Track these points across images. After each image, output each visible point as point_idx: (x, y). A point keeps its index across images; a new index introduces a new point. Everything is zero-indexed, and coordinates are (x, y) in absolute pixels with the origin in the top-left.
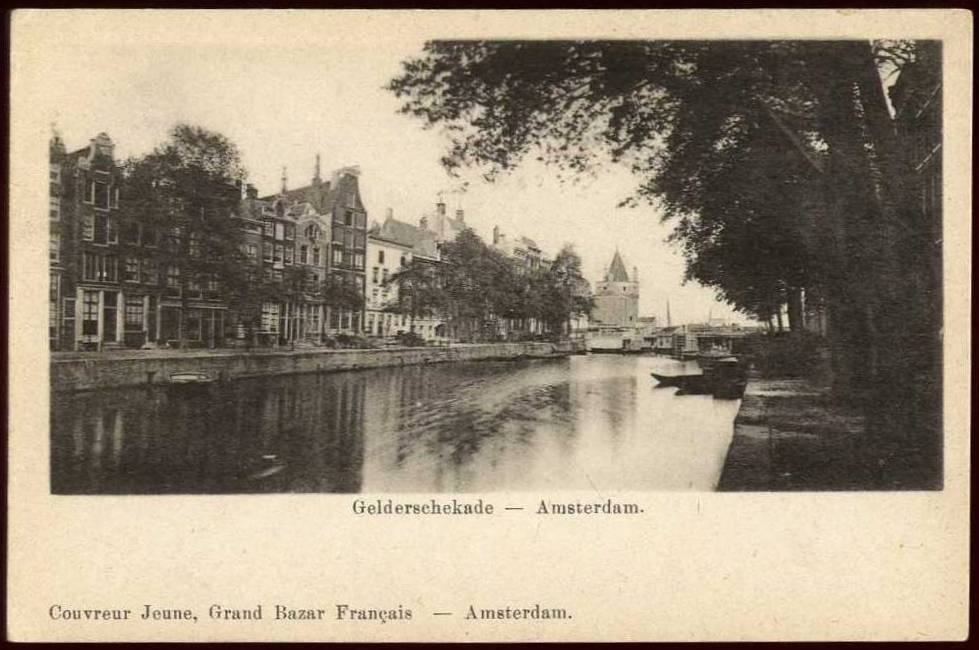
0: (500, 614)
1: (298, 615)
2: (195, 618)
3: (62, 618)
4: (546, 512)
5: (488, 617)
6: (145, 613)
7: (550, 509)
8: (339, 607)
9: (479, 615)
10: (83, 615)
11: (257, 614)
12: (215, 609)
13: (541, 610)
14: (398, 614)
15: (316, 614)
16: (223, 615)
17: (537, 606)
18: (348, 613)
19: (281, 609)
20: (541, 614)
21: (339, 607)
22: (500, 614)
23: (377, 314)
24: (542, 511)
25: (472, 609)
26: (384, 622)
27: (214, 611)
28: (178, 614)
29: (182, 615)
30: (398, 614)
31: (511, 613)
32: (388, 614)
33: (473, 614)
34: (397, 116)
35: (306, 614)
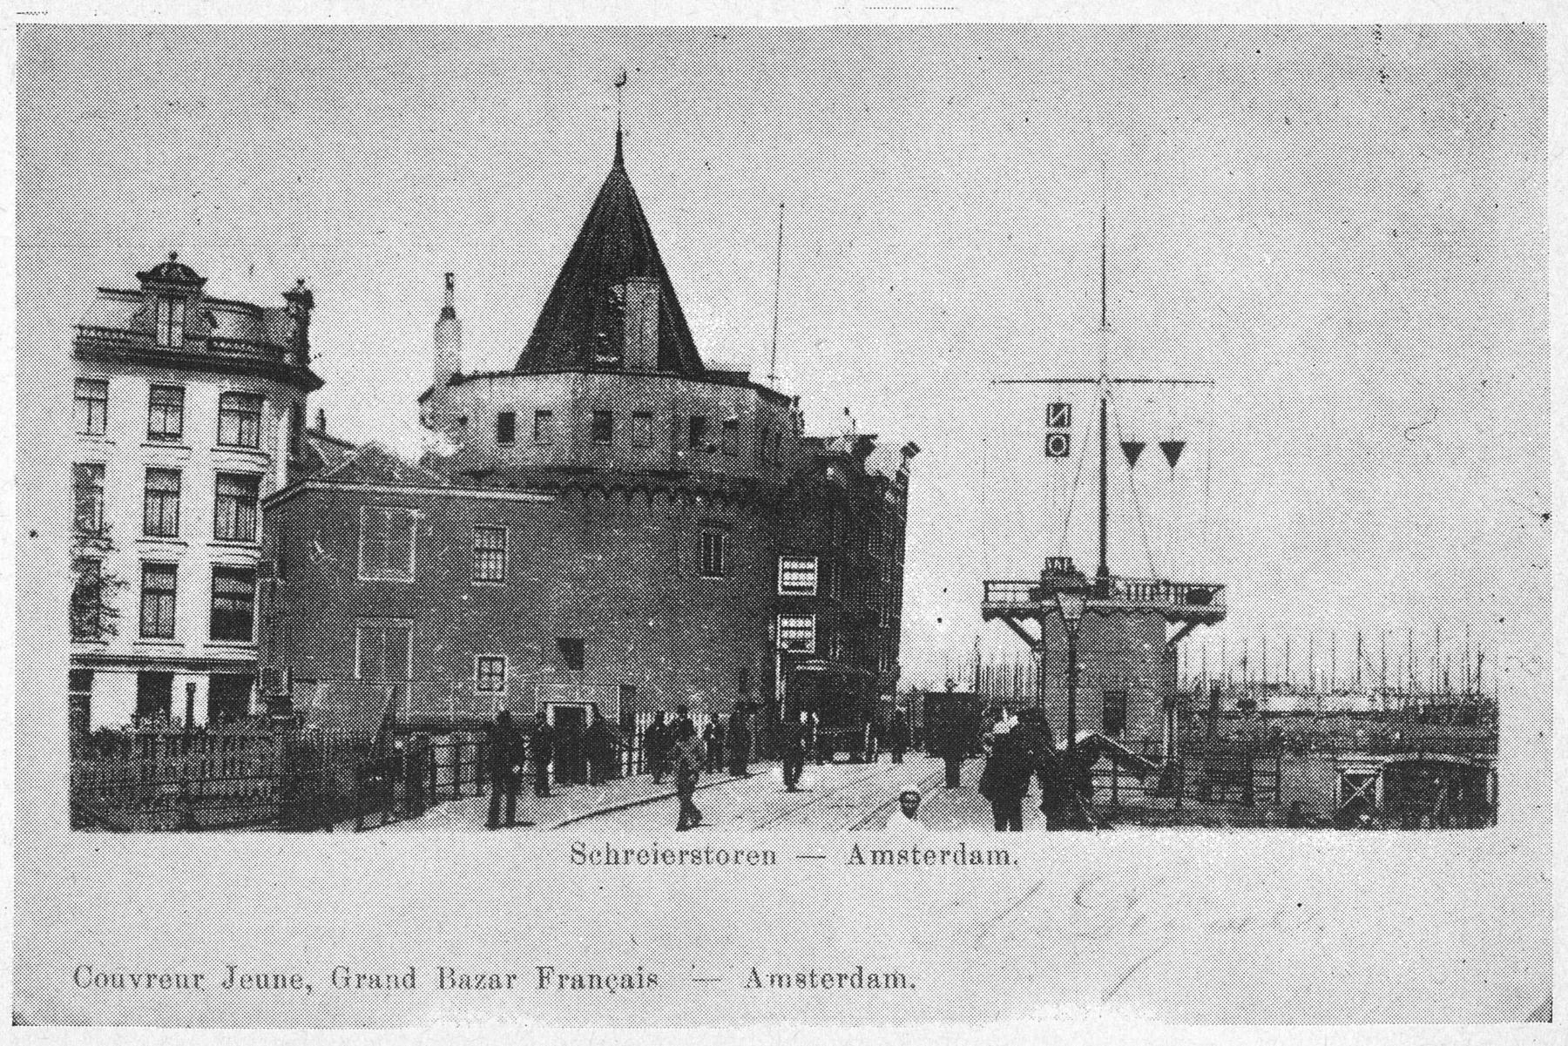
0: (903, 856)
1: (473, 983)
2: (309, 987)
3: (93, 985)
4: (862, 862)
5: (883, 861)
6: (228, 978)
7: (867, 857)
8: (541, 969)
9: (867, 857)
10: (128, 982)
11: (408, 979)
12: (341, 973)
13: (968, 850)
14: (636, 981)
15: (503, 980)
16: (353, 981)
17: (860, 968)
18: (555, 979)
19: (447, 973)
20: (968, 858)
21: (541, 969)
22: (903, 856)
23: (236, 774)
24: (753, 984)
25: (754, 972)
26: (612, 992)
27: (338, 975)
28: (280, 981)
29: (288, 982)
30: (636, 981)
31: (818, 980)
32: (619, 981)
33: (859, 857)
34: (168, 250)
35: (487, 980)
